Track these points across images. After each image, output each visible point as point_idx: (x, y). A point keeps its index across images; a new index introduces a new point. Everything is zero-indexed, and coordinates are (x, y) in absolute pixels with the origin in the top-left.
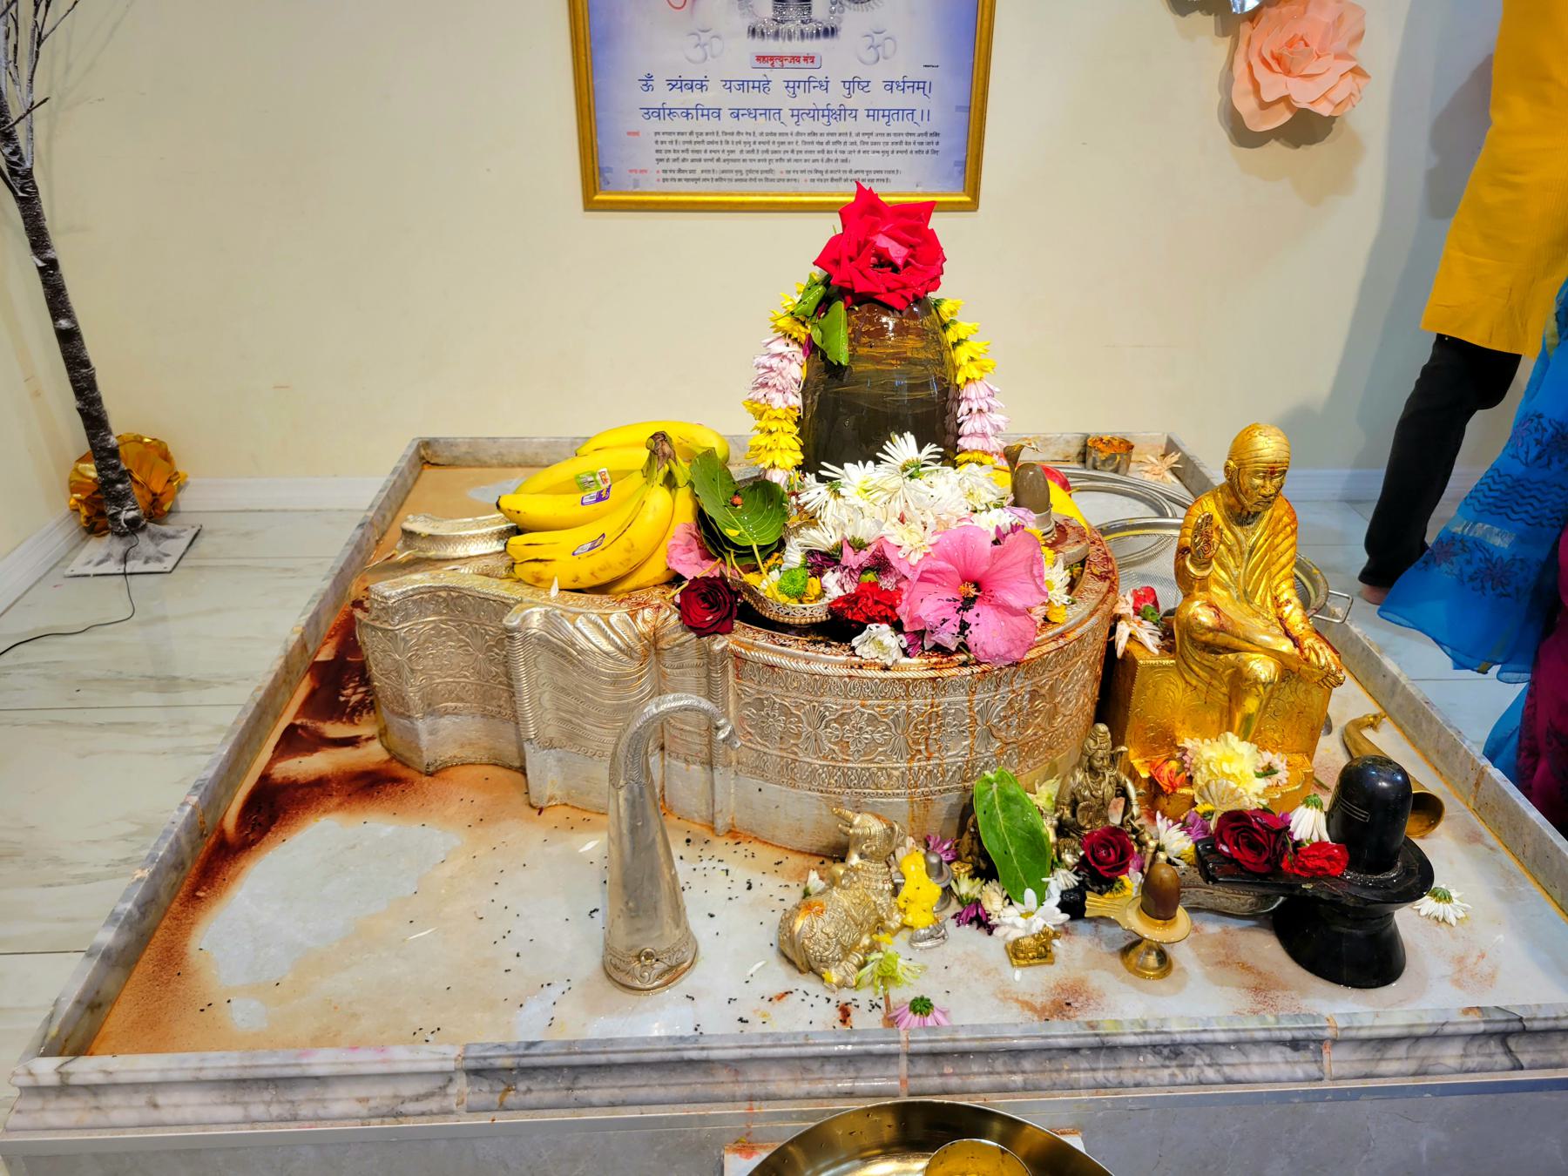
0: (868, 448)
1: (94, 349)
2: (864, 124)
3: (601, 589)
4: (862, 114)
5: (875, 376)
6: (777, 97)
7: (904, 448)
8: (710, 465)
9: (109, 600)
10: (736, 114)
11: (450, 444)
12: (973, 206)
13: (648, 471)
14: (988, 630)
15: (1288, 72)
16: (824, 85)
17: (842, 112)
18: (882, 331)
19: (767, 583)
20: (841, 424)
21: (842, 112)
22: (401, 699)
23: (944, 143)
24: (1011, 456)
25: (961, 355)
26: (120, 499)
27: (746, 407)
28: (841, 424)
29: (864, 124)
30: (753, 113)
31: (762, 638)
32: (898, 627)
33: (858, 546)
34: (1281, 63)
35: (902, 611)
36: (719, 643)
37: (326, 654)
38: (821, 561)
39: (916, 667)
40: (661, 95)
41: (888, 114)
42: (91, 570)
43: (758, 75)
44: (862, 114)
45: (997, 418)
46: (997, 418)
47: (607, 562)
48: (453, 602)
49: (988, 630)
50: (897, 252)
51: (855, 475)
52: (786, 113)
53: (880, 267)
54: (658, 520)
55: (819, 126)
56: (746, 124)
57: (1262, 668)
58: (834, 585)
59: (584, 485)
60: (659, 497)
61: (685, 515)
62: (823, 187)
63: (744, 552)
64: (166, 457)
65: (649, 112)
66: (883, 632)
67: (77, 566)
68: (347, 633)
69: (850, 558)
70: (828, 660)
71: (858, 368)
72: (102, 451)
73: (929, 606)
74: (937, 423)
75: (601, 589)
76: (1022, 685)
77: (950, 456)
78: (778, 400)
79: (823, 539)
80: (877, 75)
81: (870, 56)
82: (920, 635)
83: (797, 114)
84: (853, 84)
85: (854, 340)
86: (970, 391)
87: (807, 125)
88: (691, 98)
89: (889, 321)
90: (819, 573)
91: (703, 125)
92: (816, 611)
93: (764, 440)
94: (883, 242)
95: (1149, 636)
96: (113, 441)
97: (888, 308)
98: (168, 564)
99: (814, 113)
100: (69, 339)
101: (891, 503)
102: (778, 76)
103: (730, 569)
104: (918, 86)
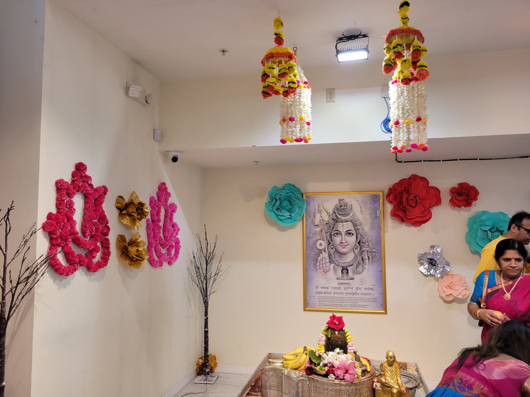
0: (333, 350)
1: (210, 335)
2: (360, 296)
3: (296, 369)
4: (360, 294)
5: (336, 340)
6: (342, 290)
7: (338, 350)
8: (312, 353)
9: (200, 388)
10: (334, 293)
11: (274, 354)
12: (386, 313)
13: (303, 353)
14: (347, 377)
15: (451, 289)
16: (352, 288)
17: (355, 294)
18: (335, 333)
19: (318, 368)
20: (330, 346)
21: (355, 294)
22: (266, 386)
23: (378, 300)
24: (355, 353)
25: (348, 338)
26: (207, 367)
27: (317, 345)
28: (330, 346)
29: (360, 296)
30: (337, 293)
31: (316, 376)
32: (335, 375)
33: (330, 363)
34: (450, 287)
35: (335, 373)
36: (310, 376)
37: (253, 384)
38: (325, 365)
39: (337, 381)
40: (319, 290)
41: (366, 294)
42: (198, 382)
43: (338, 286)
44: (360, 294)
45: (353, 348)
46: (353, 348)
47: (296, 365)
48: (275, 370)
49: (347, 377)
50: (337, 323)
51: (331, 353)
52: (344, 294)
53: (335, 325)
54: (304, 359)
55: (351, 296)
56: (336, 295)
57: (395, 391)
58: (326, 369)
59: (294, 354)
60: (304, 356)
61: (308, 359)
62: (352, 308)
63: (315, 364)
64: (215, 359)
65: (317, 293)
66: (332, 375)
67: (196, 381)
68: (256, 382)
69: (329, 365)
70: (325, 380)
71: (332, 338)
72: (206, 356)
73: (340, 373)
74: (344, 348)
75: (296, 369)
76: (353, 387)
77: (345, 352)
78: (321, 343)
79: (326, 362)
80: (362, 287)
81: (361, 283)
82: (338, 377)
83: (346, 294)
84: (357, 288)
85: (331, 334)
86: (349, 343)
87: (349, 296)
88: (325, 290)
89: (337, 333)
90: (325, 367)
91: (327, 295)
92: (324, 373)
93: (319, 348)
94: (335, 321)
95: (378, 385)
96: (209, 354)
97: (336, 330)
98: (213, 382)
99: (350, 294)
100: (206, 332)
101: (335, 357)
102: (342, 287)
103: (313, 366)
104: (371, 289)
